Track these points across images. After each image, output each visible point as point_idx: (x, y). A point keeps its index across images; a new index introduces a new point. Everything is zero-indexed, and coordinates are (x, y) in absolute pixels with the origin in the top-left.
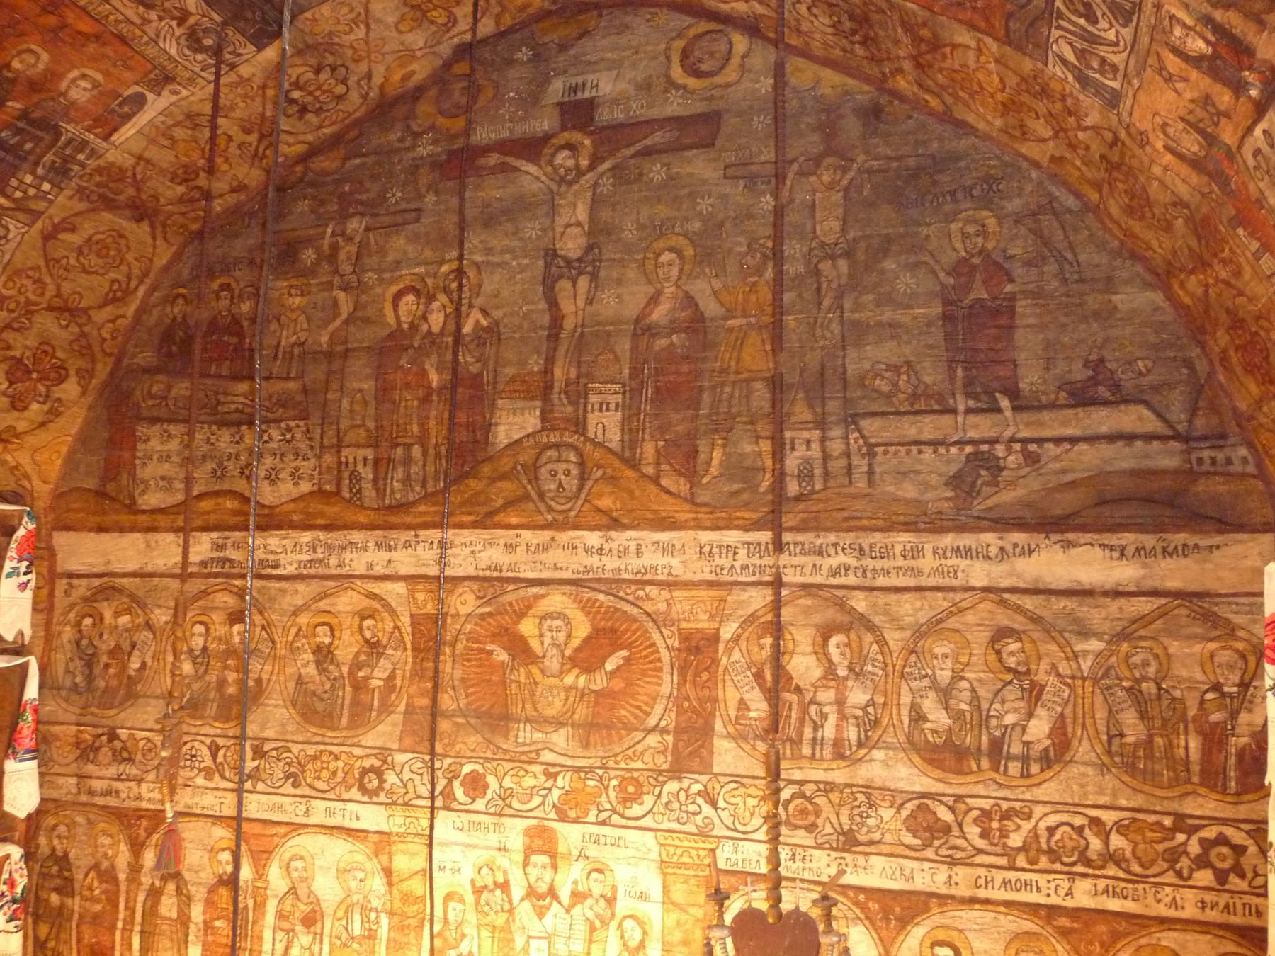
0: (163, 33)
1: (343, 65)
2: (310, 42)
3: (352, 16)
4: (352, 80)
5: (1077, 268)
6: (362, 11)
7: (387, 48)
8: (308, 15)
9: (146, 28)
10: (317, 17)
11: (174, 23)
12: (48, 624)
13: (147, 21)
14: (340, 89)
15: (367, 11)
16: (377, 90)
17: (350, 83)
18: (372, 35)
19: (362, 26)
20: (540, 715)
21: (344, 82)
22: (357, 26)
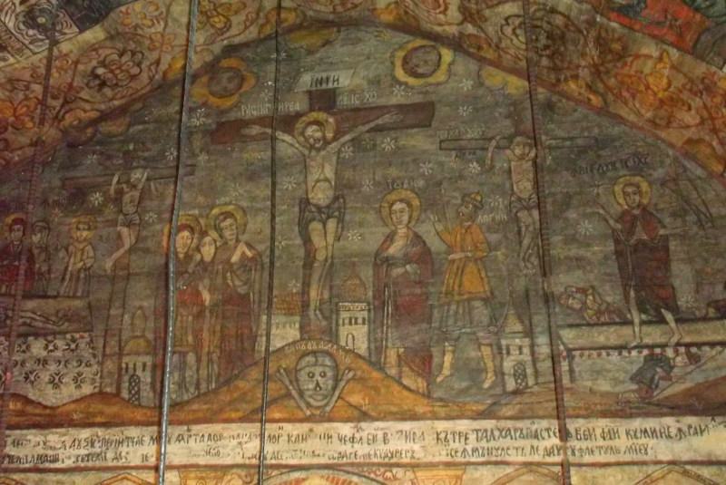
3: (157, 13)
8: (123, 9)
14: (135, 70)
15: (168, 11)
22: (159, 22)
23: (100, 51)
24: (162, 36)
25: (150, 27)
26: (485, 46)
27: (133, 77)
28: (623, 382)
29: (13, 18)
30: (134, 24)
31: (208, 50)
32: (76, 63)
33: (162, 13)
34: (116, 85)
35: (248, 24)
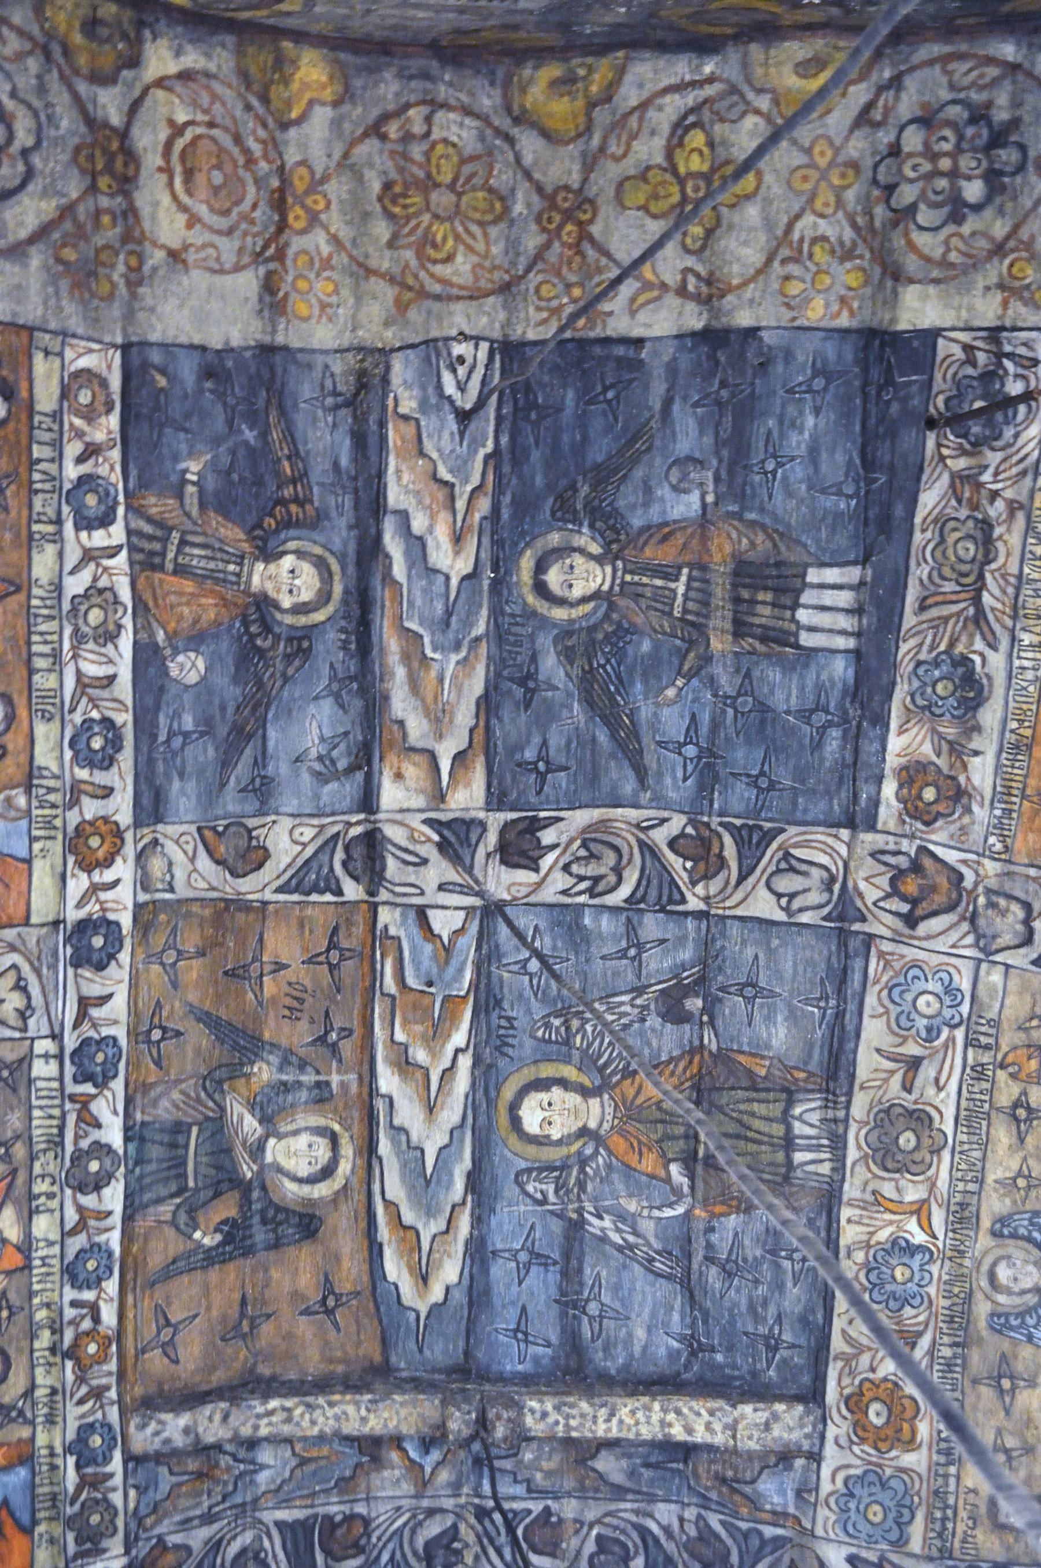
0: (1014, 471)
1: (875, 182)
2: (878, 271)
3: (794, 269)
4: (885, 137)
5: (59, 811)
6: (776, 264)
7: (798, 159)
8: (844, 321)
9: (1023, 498)
10: (835, 307)
11: (986, 477)
12: (692, 1296)
13: (1013, 507)
14: (913, 140)
15: (769, 261)
16: (874, 77)
17: (892, 137)
18: (796, 208)
19: (796, 236)
20: (886, 238)
21: (895, 151)
22: (802, 240)
23: (938, 253)
24: (811, 200)
25: (824, 239)
26: (77, 38)
27: (926, 120)
28: (76, 1143)
29: (1020, 442)
30: (848, 265)
31: (749, 81)
32: (999, 250)
33: (784, 262)
34: (973, 120)
35: (633, 122)
